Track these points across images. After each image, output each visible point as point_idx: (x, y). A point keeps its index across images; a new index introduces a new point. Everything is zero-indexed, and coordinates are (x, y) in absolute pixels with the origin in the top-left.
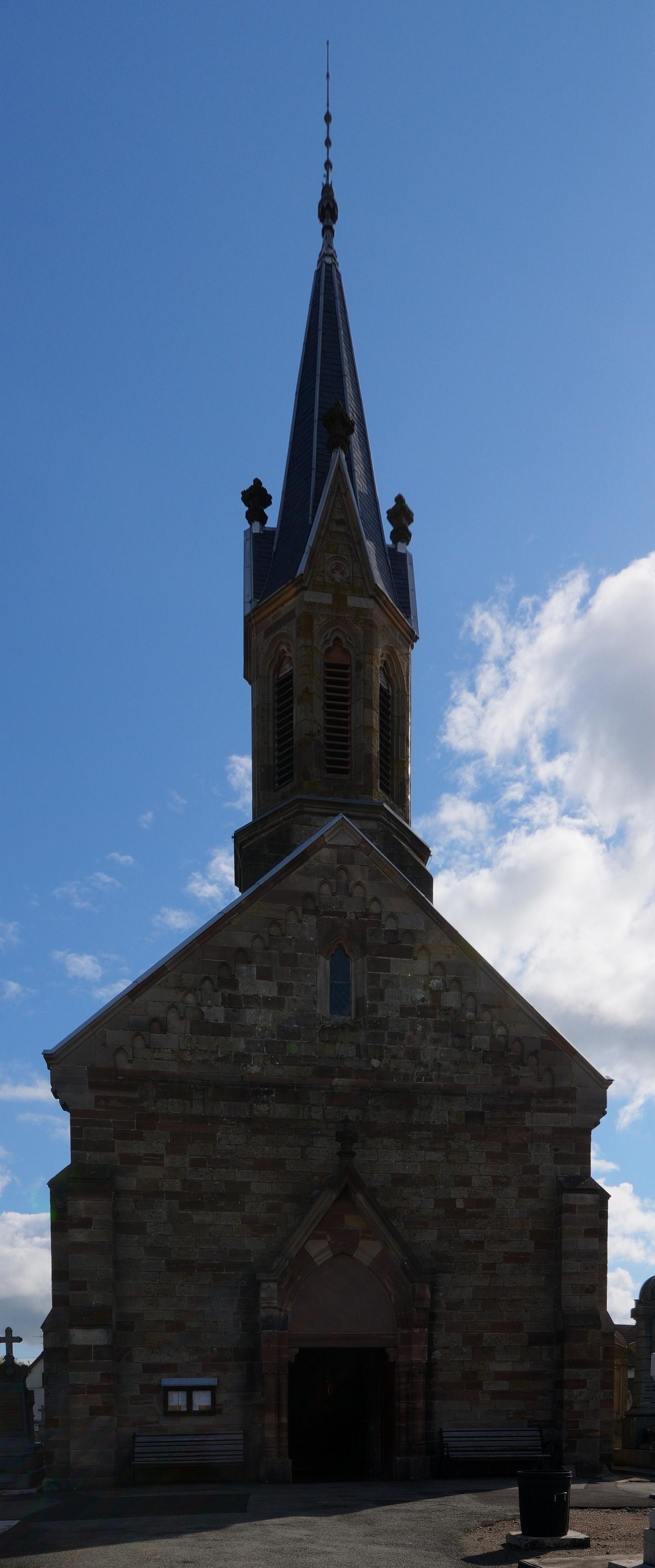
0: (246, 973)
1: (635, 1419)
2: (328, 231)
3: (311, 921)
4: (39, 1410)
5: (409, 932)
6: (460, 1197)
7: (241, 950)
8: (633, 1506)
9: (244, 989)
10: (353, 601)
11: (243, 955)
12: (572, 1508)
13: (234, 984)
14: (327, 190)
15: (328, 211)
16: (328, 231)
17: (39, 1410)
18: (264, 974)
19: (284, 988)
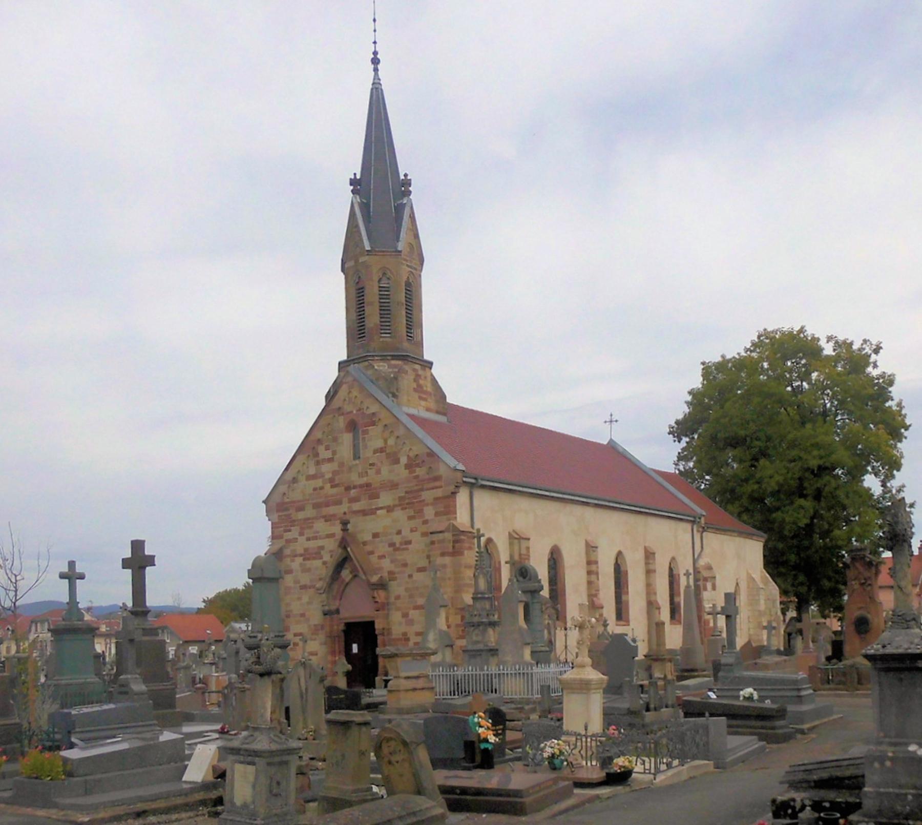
0: (321, 449)
1: (815, 521)
2: (376, 70)
3: (341, 419)
4: (506, 563)
5: (373, 414)
6: (397, 539)
7: (319, 440)
8: (186, 782)
9: (321, 457)
10: (362, 260)
11: (319, 441)
12: (881, 587)
13: (317, 455)
14: (375, 53)
15: (375, 61)
16: (376, 70)
17: (506, 563)
18: (327, 448)
19: (334, 453)
